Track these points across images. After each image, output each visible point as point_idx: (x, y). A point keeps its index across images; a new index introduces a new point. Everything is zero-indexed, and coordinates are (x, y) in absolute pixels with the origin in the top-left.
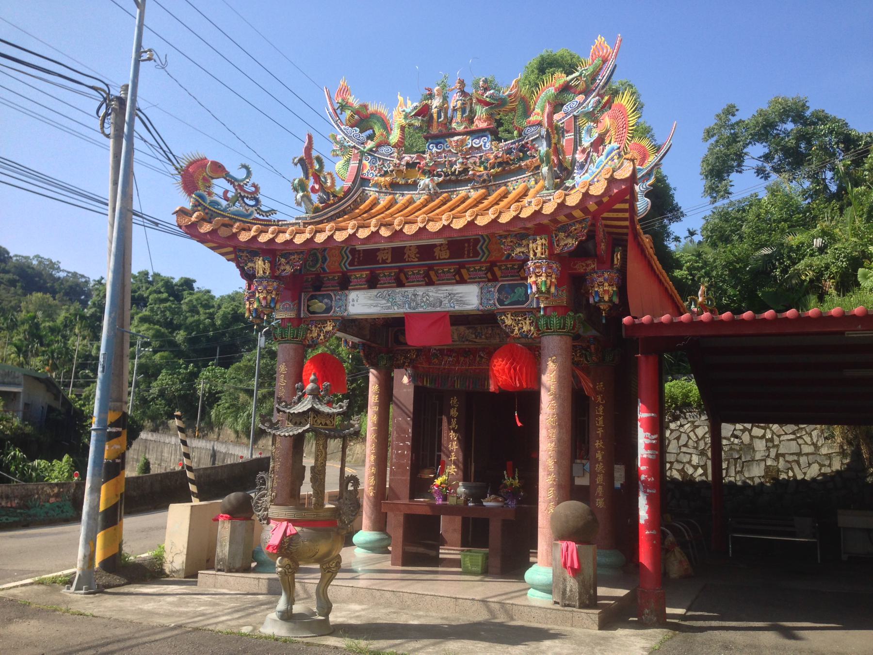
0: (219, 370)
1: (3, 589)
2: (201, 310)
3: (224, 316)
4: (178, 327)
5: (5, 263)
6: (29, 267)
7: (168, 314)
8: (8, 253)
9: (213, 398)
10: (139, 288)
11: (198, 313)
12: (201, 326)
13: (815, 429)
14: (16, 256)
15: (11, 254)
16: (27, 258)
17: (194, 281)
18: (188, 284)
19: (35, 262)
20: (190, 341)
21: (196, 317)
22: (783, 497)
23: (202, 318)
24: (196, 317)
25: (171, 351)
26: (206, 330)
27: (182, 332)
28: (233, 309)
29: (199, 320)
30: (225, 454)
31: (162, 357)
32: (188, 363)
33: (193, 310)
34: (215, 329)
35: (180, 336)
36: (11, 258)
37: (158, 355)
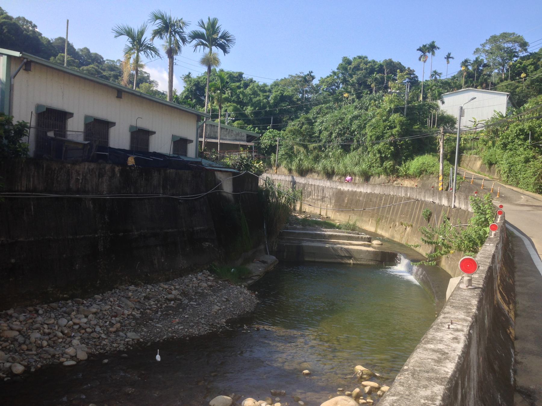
0: (276, 132)
1: (2, 195)
2: (261, 94)
3: (276, 97)
4: (246, 104)
5: (436, 110)
6: (115, 67)
7: (241, 96)
8: (103, 59)
9: (272, 149)
10: (213, 79)
11: (259, 95)
12: (262, 104)
13: (231, 105)
14: (107, 60)
15: (105, 59)
16: (113, 61)
17: (243, 74)
18: (240, 75)
19: (118, 64)
20: (256, 114)
21: (258, 98)
22: (275, 194)
23: (261, 98)
24: (258, 98)
25: (243, 120)
26: (264, 107)
27: (249, 108)
28: (281, 93)
29: (260, 100)
30: (304, 185)
31: (238, 124)
32: (255, 127)
33: (255, 93)
34: (270, 107)
35: (249, 110)
36: (104, 61)
37: (236, 122)
